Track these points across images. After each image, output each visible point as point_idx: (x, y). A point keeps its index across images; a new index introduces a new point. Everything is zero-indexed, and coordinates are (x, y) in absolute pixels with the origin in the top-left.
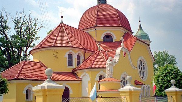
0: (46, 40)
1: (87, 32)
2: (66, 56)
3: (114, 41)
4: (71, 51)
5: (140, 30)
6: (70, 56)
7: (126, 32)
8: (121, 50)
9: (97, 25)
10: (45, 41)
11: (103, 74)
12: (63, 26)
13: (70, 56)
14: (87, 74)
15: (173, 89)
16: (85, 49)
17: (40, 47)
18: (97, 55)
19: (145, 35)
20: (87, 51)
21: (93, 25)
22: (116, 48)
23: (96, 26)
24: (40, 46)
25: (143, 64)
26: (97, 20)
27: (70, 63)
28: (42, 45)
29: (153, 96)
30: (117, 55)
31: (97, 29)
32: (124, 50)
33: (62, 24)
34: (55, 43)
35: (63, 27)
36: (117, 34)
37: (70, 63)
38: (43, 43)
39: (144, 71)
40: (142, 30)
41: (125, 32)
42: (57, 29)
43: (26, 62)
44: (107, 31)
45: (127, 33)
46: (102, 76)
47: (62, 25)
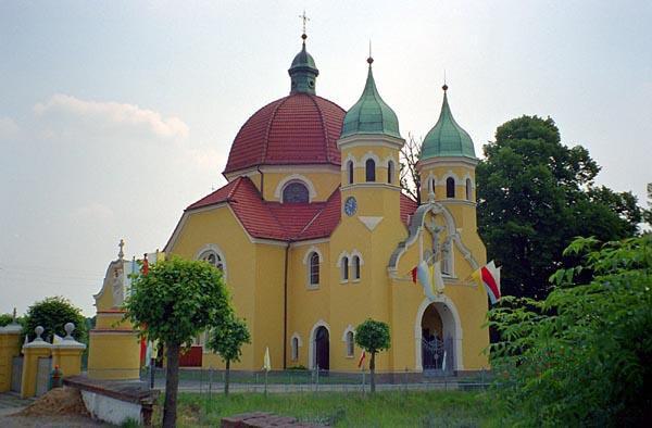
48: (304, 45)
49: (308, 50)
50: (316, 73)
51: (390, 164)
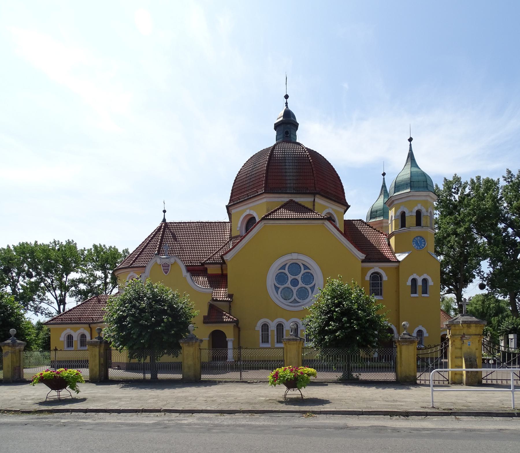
48: (287, 103)
49: (290, 108)
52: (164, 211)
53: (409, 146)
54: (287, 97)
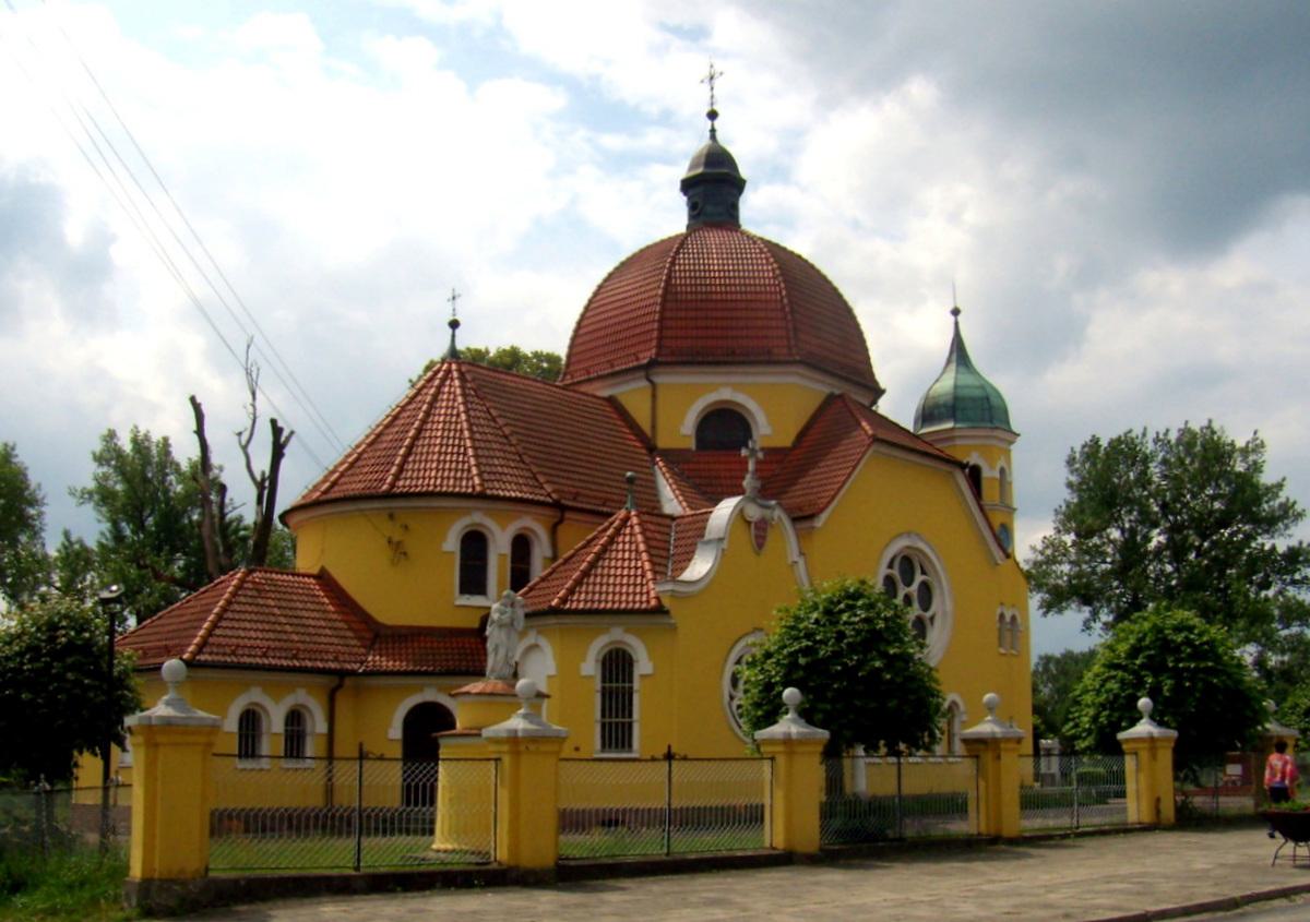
0: (360, 454)
1: (606, 393)
2: (452, 543)
3: (898, 406)
4: (477, 518)
5: (953, 366)
6: (474, 544)
7: (837, 392)
8: (739, 513)
9: (658, 354)
10: (352, 465)
11: (625, 643)
12: (455, 374)
13: (474, 544)
14: (543, 641)
15: (1144, 728)
16: (556, 505)
17: (325, 497)
18: (612, 540)
19: (978, 393)
20: (568, 515)
21: (641, 356)
22: (716, 502)
23: (652, 364)
24: (325, 493)
25: (919, 578)
26: (661, 329)
27: (473, 580)
28: (334, 484)
29: (653, 759)
30: (709, 542)
31: (664, 379)
32: (754, 512)
33: (454, 367)
34: (397, 477)
35: (457, 383)
36: (775, 407)
37: (473, 580)
38: (342, 475)
39: (928, 614)
40: (962, 369)
41: (827, 390)
42: (425, 391)
43: (250, 578)
44: (714, 388)
45: (840, 396)
46: (617, 650)
47: (449, 371)
48: (713, 131)
50: (688, 186)
51: (1002, 471)
52: (454, 325)
53: (449, 338)
54: (713, 115)
